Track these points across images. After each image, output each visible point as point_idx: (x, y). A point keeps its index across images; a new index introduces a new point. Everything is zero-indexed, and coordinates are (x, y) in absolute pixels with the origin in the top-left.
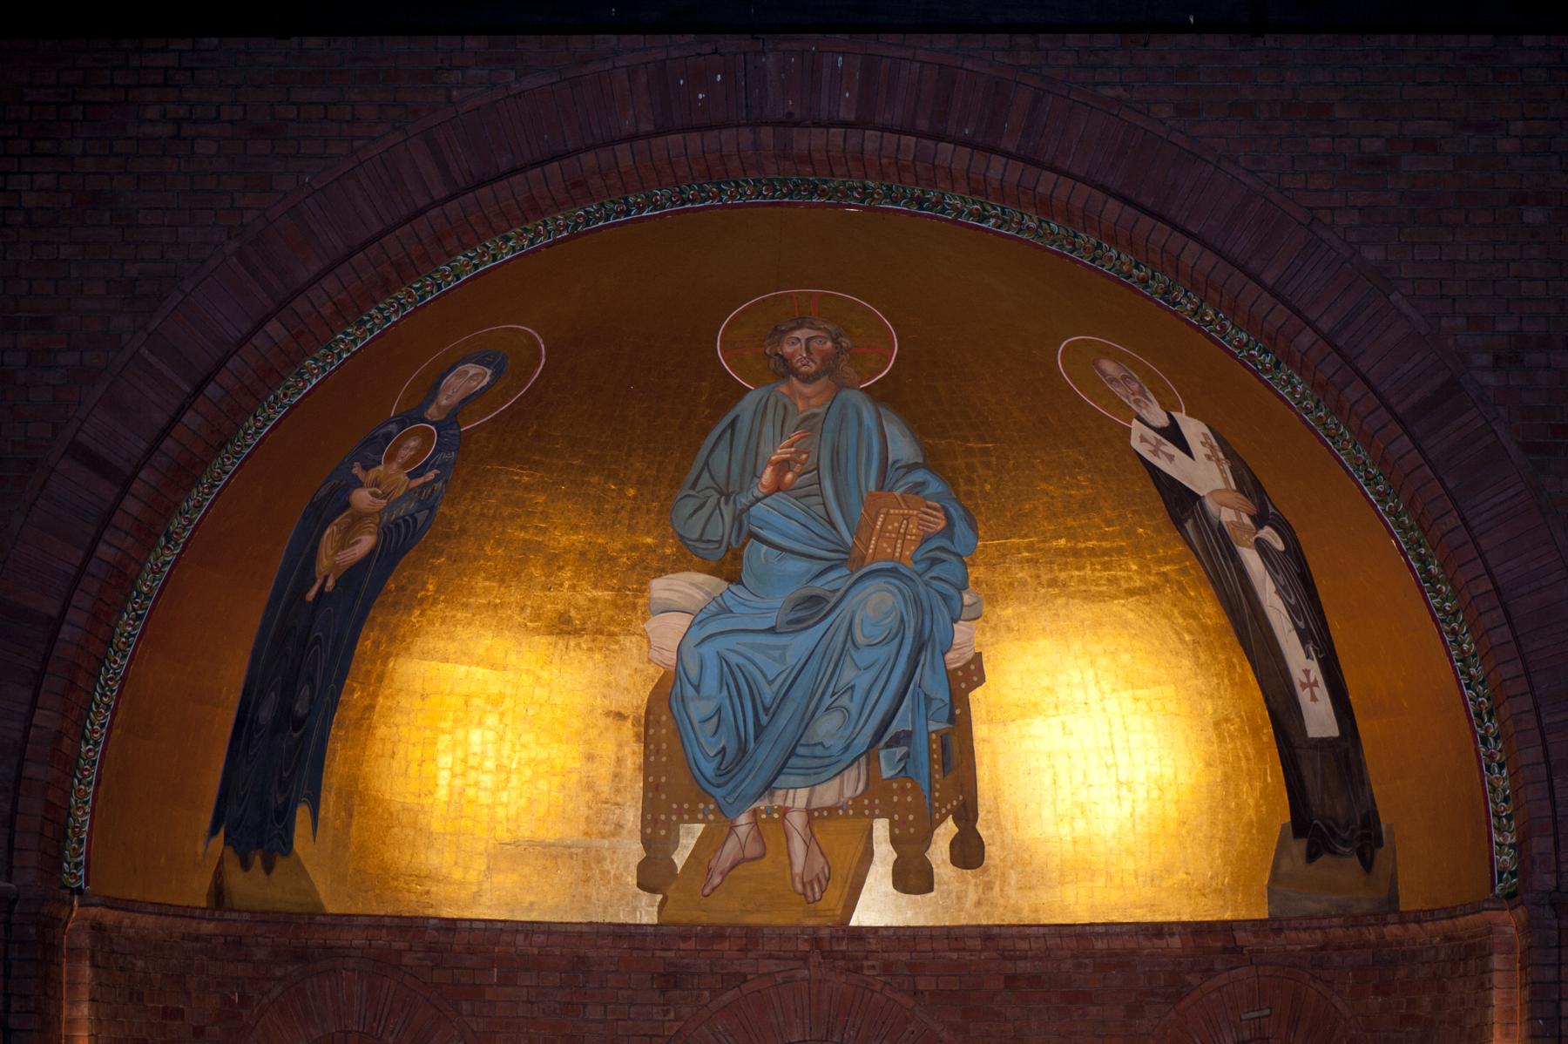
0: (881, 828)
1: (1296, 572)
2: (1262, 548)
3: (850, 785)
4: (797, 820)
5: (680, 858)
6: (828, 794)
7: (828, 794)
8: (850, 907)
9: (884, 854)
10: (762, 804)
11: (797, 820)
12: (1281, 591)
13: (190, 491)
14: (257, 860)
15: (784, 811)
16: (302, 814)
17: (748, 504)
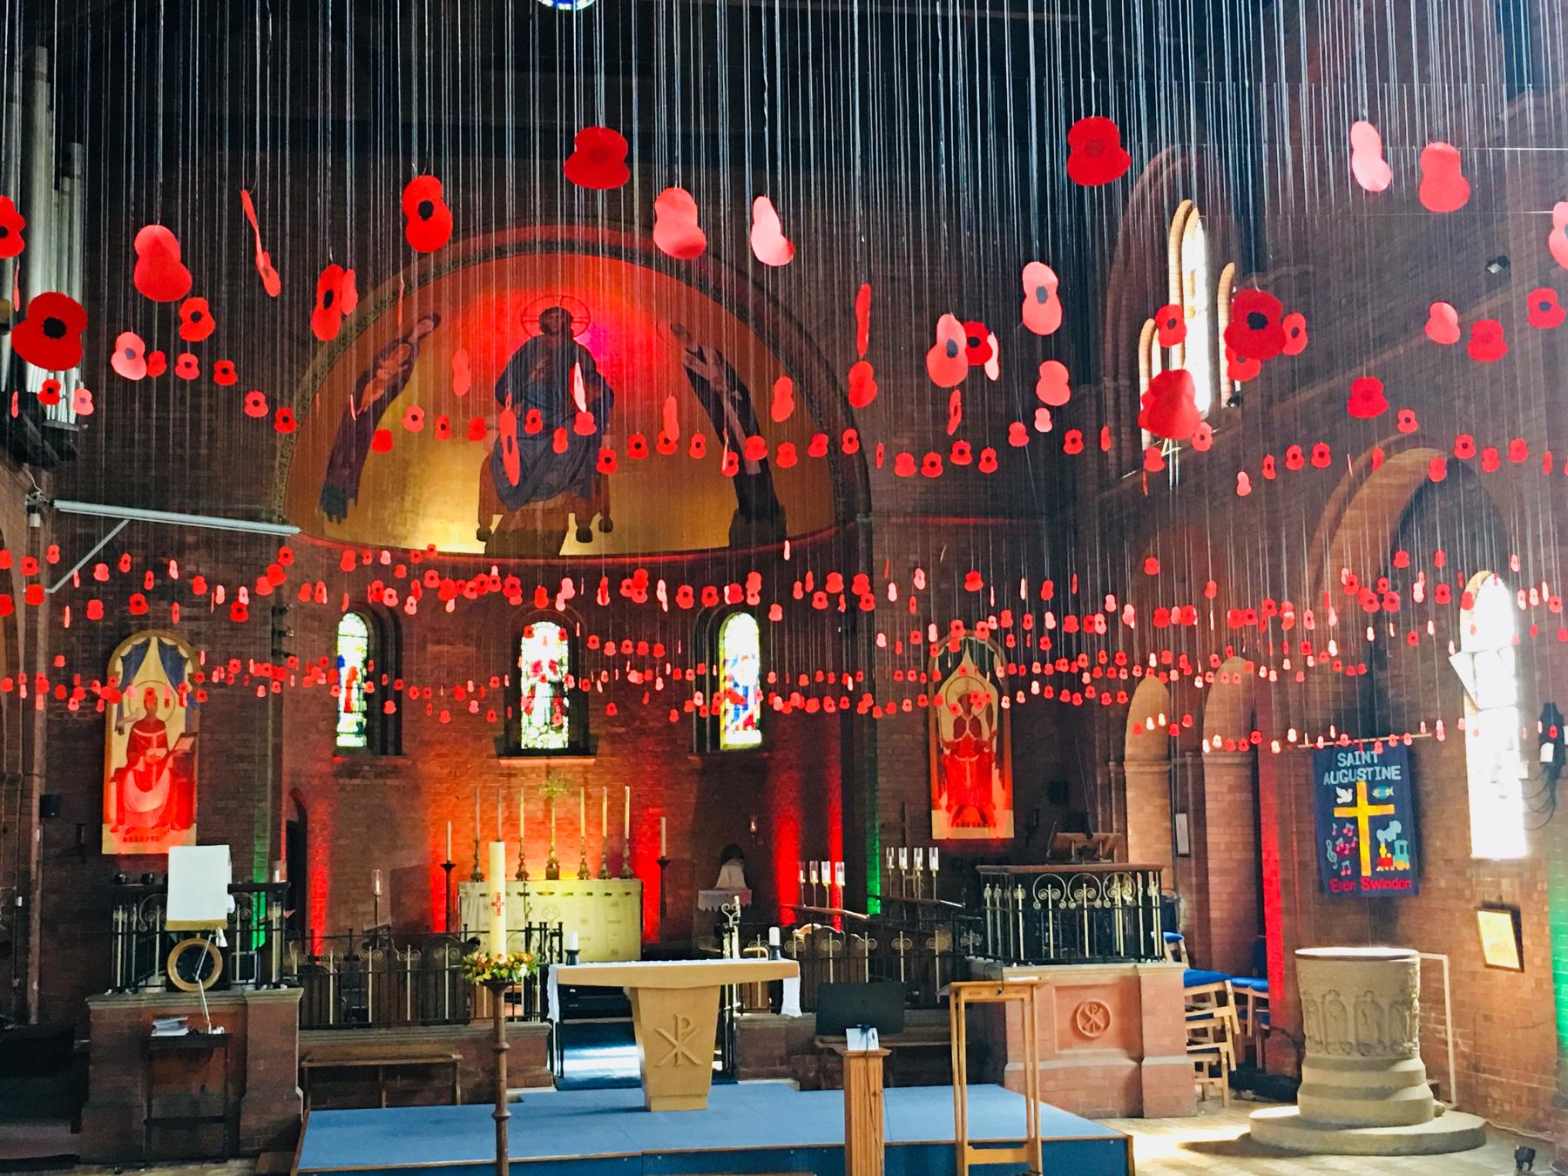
0: (572, 517)
1: (1200, 545)
2: (733, 400)
3: (558, 500)
4: (539, 514)
5: (493, 528)
6: (551, 504)
7: (551, 504)
8: (559, 550)
9: (573, 527)
10: (524, 508)
11: (539, 514)
12: (83, 203)
13: (89, 1011)
14: (335, 520)
15: (534, 511)
16: (351, 501)
17: (1250, 759)
